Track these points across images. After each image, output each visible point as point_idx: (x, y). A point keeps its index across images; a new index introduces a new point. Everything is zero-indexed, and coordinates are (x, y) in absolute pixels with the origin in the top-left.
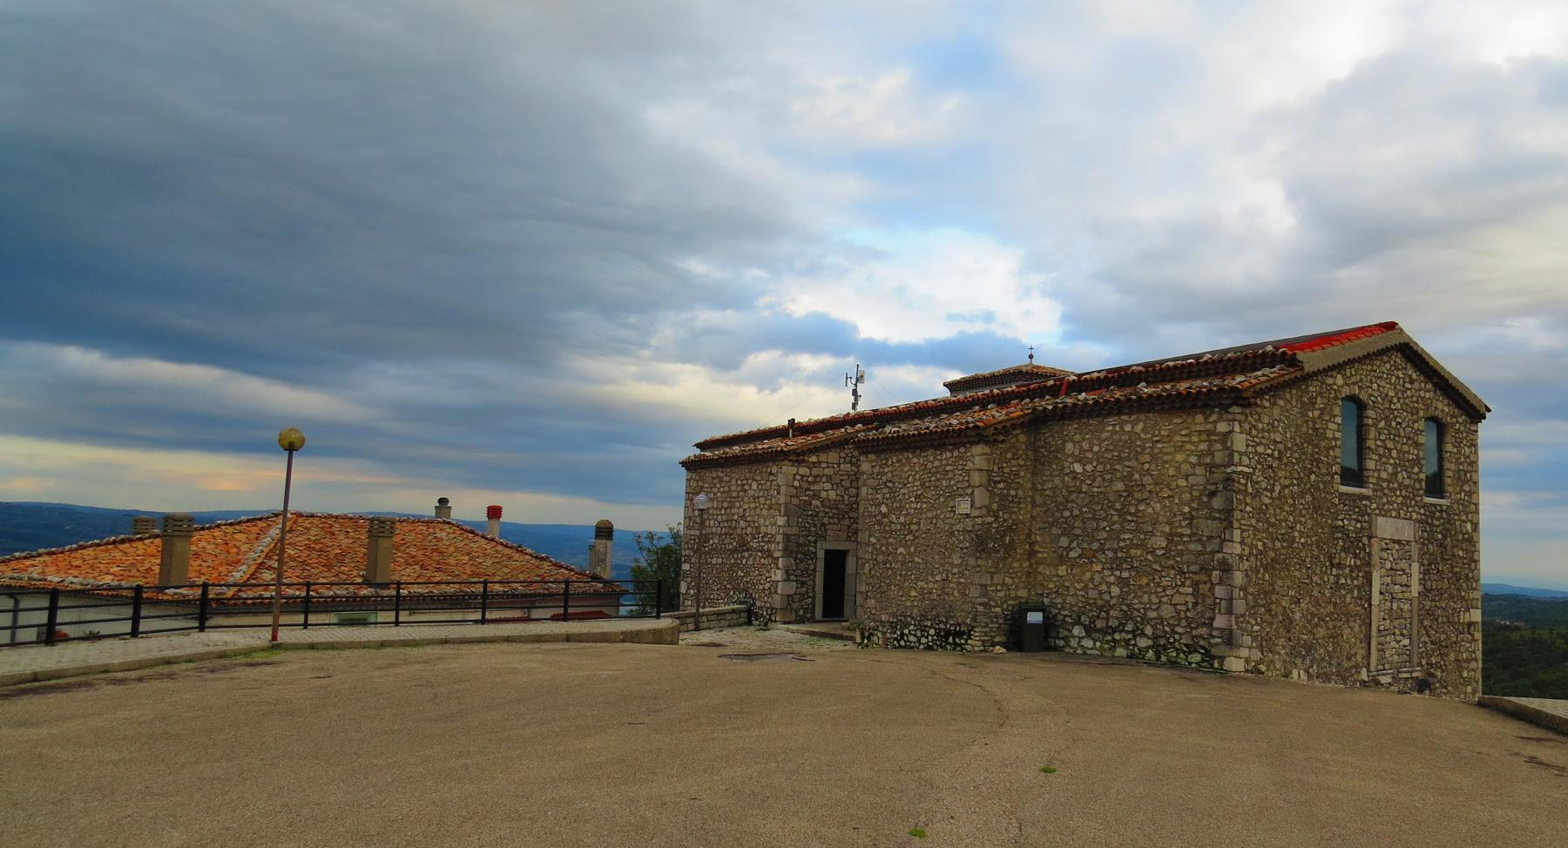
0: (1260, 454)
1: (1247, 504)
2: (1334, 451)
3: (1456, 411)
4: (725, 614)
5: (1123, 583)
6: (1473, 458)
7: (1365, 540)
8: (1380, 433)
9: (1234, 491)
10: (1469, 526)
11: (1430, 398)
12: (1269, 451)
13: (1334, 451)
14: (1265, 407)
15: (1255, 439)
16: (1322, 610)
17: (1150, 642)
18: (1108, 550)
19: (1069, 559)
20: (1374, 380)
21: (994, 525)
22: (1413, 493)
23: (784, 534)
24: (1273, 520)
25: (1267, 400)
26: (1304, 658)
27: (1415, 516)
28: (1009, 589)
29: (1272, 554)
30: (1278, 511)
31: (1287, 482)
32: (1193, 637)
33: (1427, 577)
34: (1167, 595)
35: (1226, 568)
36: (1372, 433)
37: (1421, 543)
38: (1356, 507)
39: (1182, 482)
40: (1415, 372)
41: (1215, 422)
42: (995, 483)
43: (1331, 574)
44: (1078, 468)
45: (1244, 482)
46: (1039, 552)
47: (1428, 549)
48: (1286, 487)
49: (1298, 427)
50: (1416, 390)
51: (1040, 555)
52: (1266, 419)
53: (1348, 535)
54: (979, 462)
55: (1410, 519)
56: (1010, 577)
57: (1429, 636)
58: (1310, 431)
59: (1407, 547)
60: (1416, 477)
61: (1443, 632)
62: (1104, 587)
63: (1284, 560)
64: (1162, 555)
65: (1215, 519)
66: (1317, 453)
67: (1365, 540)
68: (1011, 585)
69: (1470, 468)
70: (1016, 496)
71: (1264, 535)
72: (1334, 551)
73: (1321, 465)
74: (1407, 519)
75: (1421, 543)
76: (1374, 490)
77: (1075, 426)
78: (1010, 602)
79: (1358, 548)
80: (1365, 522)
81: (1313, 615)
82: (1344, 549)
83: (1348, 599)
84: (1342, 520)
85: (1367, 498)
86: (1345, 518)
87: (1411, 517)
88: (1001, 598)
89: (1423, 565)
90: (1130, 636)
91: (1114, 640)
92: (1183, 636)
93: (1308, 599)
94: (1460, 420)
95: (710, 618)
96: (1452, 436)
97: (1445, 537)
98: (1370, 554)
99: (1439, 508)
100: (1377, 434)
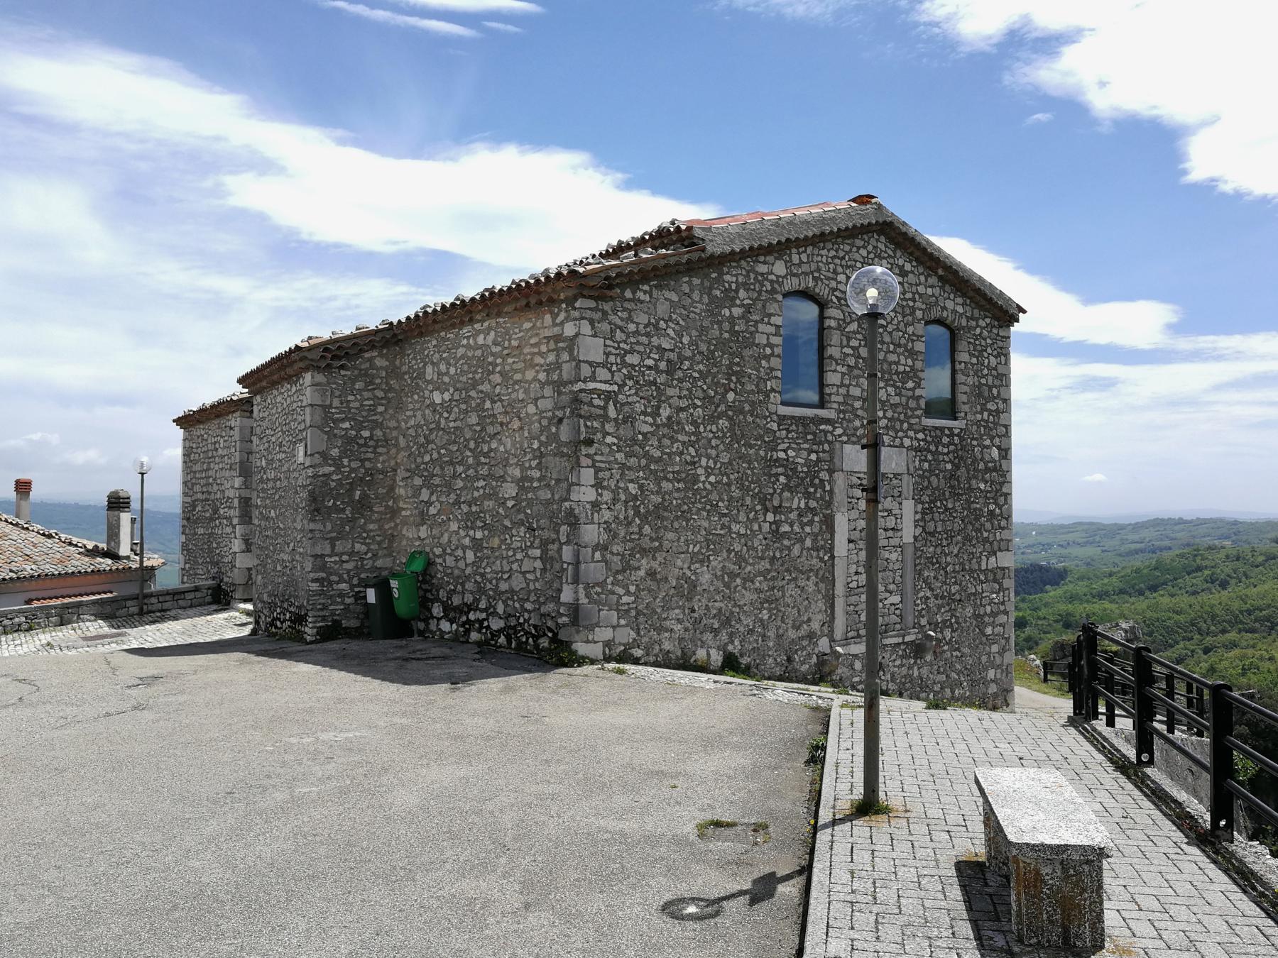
0: (633, 366)
1: (607, 434)
2: (768, 361)
3: (976, 311)
4: (184, 593)
5: (477, 545)
6: (1001, 369)
7: (824, 475)
8: (849, 339)
9: (581, 416)
10: (995, 453)
11: (933, 295)
12: (650, 362)
13: (768, 361)
14: (642, 302)
15: (622, 345)
16: (749, 568)
17: (501, 624)
18: (464, 502)
19: (429, 516)
20: (840, 269)
21: (334, 477)
22: (906, 414)
23: (240, 498)
24: (657, 454)
25: (645, 292)
26: (716, 632)
27: (907, 442)
28: (362, 559)
29: (656, 499)
30: (666, 442)
31: (684, 403)
32: (542, 615)
33: (928, 518)
34: (517, 560)
35: (573, 522)
36: (835, 338)
37: (919, 476)
38: (809, 433)
39: (531, 409)
40: (910, 262)
41: (562, 323)
42: (336, 421)
43: (765, 521)
44: (437, 398)
45: (602, 403)
46: (404, 509)
47: (929, 482)
48: (682, 409)
49: (703, 330)
50: (911, 284)
51: (404, 513)
52: (643, 319)
53: (794, 470)
54: (309, 396)
55: (902, 446)
56: (362, 544)
57: (931, 589)
58: (726, 335)
59: (895, 482)
60: (910, 393)
61: (955, 583)
62: (459, 553)
63: (679, 506)
64: (513, 506)
65: (562, 455)
66: (738, 364)
67: (824, 475)
68: (366, 554)
69: (997, 382)
70: (371, 438)
71: (641, 474)
72: (771, 491)
73: (745, 380)
74: (897, 447)
75: (919, 476)
76: (840, 411)
77: (434, 342)
78: (363, 576)
79: (813, 485)
80: (824, 451)
81: (733, 576)
82: (787, 487)
83: (796, 550)
84: (785, 451)
85: (827, 421)
86: (789, 448)
87: (902, 443)
88: (348, 572)
89: (923, 503)
90: (484, 615)
91: (468, 621)
92: (532, 615)
93: (725, 554)
94: (982, 323)
95: (161, 599)
96: (969, 343)
97: (957, 467)
98: (831, 492)
99: (947, 432)
100: (844, 339)
